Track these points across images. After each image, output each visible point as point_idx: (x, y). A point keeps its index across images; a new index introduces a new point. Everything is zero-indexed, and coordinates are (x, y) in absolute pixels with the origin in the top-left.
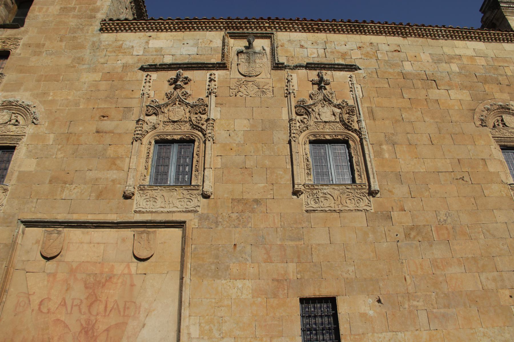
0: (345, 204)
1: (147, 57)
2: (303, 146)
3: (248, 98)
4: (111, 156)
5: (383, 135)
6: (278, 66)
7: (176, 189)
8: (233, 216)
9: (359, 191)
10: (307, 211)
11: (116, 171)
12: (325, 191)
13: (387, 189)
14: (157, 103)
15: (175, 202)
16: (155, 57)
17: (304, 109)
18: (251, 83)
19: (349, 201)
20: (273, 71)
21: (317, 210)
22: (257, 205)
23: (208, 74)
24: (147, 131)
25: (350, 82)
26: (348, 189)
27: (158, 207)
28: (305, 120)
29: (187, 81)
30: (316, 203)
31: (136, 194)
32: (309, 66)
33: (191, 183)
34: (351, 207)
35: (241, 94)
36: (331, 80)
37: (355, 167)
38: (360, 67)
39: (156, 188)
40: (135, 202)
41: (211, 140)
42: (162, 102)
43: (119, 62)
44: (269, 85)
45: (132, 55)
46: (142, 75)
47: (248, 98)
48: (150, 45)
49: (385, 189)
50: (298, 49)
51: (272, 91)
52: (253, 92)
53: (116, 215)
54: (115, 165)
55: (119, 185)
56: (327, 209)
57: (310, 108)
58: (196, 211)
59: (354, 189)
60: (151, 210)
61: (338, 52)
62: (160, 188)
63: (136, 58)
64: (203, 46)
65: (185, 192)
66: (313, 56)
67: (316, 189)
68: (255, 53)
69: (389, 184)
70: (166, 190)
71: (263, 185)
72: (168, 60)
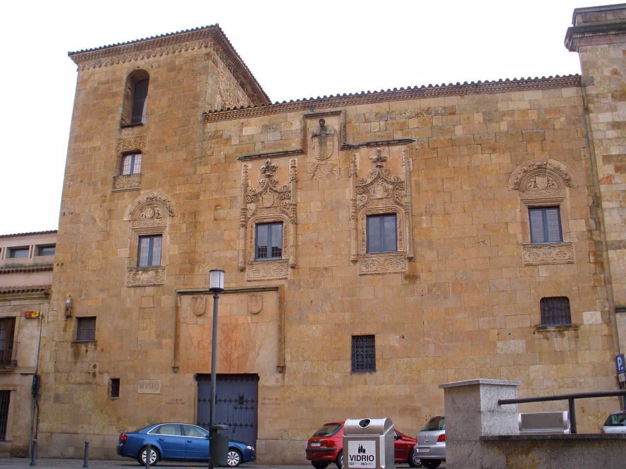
1: (242, 146)
16: (249, 145)
17: (363, 188)
18: (323, 166)
20: (341, 152)
22: (326, 272)
29: (274, 169)
34: (391, 270)
40: (246, 274)
43: (222, 153)
45: (231, 145)
49: (419, 255)
50: (363, 124)
51: (339, 173)
59: (394, 256)
61: (398, 123)
63: (234, 148)
65: (279, 265)
66: (374, 131)
72: (259, 149)
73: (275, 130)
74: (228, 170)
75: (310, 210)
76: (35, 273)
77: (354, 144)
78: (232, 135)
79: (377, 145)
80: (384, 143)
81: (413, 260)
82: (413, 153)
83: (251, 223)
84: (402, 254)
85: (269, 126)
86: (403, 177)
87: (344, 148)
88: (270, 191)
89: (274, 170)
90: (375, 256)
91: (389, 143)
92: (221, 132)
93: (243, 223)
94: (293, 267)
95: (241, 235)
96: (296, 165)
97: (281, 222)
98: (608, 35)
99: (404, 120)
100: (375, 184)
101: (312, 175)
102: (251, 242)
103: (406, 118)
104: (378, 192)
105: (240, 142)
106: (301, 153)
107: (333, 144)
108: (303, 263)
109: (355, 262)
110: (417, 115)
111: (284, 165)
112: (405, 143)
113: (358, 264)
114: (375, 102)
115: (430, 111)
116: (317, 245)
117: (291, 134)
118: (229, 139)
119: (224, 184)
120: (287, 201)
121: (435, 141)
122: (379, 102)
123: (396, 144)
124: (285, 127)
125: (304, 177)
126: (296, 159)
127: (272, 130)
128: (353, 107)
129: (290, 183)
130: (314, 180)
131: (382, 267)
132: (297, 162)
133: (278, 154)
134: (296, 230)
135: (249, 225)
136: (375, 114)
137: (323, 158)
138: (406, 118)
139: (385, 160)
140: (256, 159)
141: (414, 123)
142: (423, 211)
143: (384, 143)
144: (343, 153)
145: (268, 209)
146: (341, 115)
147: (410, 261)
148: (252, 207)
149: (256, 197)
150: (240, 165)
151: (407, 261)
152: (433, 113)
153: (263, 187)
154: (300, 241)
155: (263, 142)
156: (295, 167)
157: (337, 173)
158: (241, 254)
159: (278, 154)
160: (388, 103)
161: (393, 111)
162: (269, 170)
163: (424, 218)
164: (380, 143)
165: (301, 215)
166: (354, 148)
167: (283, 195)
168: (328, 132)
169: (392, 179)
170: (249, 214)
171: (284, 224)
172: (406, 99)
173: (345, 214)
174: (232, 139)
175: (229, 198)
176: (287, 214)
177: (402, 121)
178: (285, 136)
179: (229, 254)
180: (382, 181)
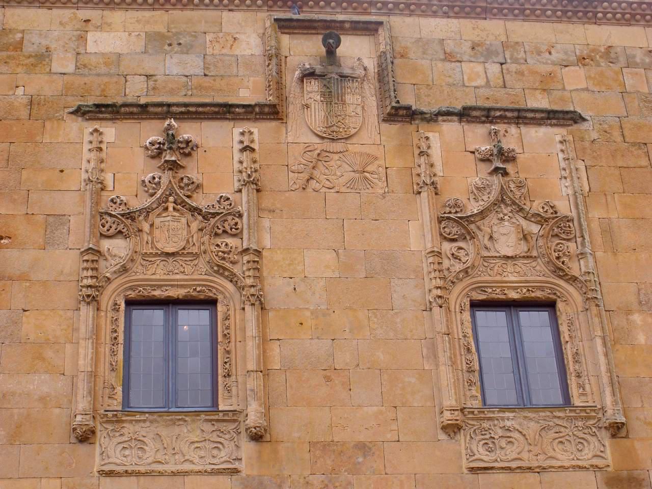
0: (552, 453)
1: (86, 80)
2: (458, 315)
3: (331, 195)
4: (31, 340)
5: (633, 288)
6: (402, 114)
7: (187, 419)
8: (315, 482)
9: (580, 424)
10: (472, 470)
11: (47, 376)
12: (508, 423)
13: (642, 417)
14: (122, 207)
15: (185, 449)
16: (106, 79)
17: (457, 225)
18: (336, 157)
19: (560, 446)
20: (385, 126)
21: (492, 468)
22: (365, 456)
23: (237, 131)
24: (109, 279)
25: (561, 156)
26: (555, 417)
27: (150, 460)
28: (462, 253)
29: (188, 149)
30: (490, 451)
31: (98, 434)
32: (465, 115)
33: (215, 403)
34: (564, 459)
35: (317, 186)
36: (518, 150)
37: (571, 367)
38: (583, 115)
39: (143, 418)
40: (98, 451)
41: (257, 303)
42: (136, 204)
43: (20, 91)
44: (377, 162)
45: (50, 72)
46: (81, 131)
47: (331, 195)
48: (91, 48)
49: (637, 419)
50: (440, 64)
51: (384, 179)
52: (342, 181)
53: (58, 481)
54: (44, 359)
55: (57, 411)
56: (514, 465)
57: (473, 222)
58: (236, 471)
59: (569, 418)
60: (137, 468)
61: (533, 72)
62: (151, 417)
63: (59, 82)
64: (216, 52)
65: (208, 427)
66: (474, 84)
67: (489, 419)
68: (343, 77)
69: (645, 405)
70: (166, 421)
71: (375, 409)
72: (136, 91)
73: (186, 49)
74: (38, 138)
75: (304, 271)
76: (245, 121)
77: (424, 109)
78: (53, 46)
79: (488, 117)
80: (509, 114)
81: (623, 433)
82: (584, 149)
83: (113, 295)
84: (588, 413)
85: (168, 38)
86: (564, 208)
87: (396, 115)
88: (174, 209)
89: (187, 151)
90: (511, 415)
91: (521, 117)
92: (19, 35)
93: (89, 292)
94: (257, 438)
95: (83, 329)
96: (256, 146)
97: (210, 303)
98: (561, 21)
99: (549, 68)
100: (492, 219)
101: (305, 176)
102: (113, 353)
103: (553, 64)
104: (503, 239)
105: (77, 67)
106: (269, 114)
107: (362, 105)
108: (289, 424)
109: (452, 429)
110: (582, 60)
111: (217, 140)
112: (562, 122)
113: (461, 437)
114: (467, 16)
115: (613, 55)
116: (330, 373)
117: (234, 65)
118: (42, 58)
119: (24, 177)
120: (231, 241)
121: (639, 127)
122: (478, 16)
123: (538, 122)
124: (217, 46)
125: (277, 179)
126: (255, 131)
127: (177, 48)
128: (409, 20)
129: (240, 191)
130: (309, 190)
131: (536, 450)
132: (256, 136)
133: (201, 109)
134: (262, 324)
135: (106, 300)
136: (469, 44)
137: (333, 135)
138: (553, 64)
139: (513, 159)
140: (130, 116)
141: (575, 79)
142: (633, 299)
143: (509, 114)
144: (393, 129)
145: (171, 259)
146: (380, 31)
147: (614, 436)
148: (118, 248)
149: (126, 222)
150: (80, 131)
151: (605, 436)
152: (622, 60)
153: (152, 195)
154: (277, 359)
155: (148, 77)
156: (253, 150)
157: (380, 179)
158: (82, 387)
159: (201, 109)
160: (501, 22)
161: (517, 43)
162: (173, 154)
163: (637, 318)
164: (498, 114)
165: (276, 287)
166: (423, 119)
167: (220, 221)
168: (347, 71)
169: (536, 206)
170: (107, 268)
171: (220, 308)
172: (548, 19)
173: (409, 293)
174: (55, 57)
175: (40, 218)
176: (232, 278)
177: (544, 69)
178: (215, 66)
179: (40, 384)
180: (511, 212)
